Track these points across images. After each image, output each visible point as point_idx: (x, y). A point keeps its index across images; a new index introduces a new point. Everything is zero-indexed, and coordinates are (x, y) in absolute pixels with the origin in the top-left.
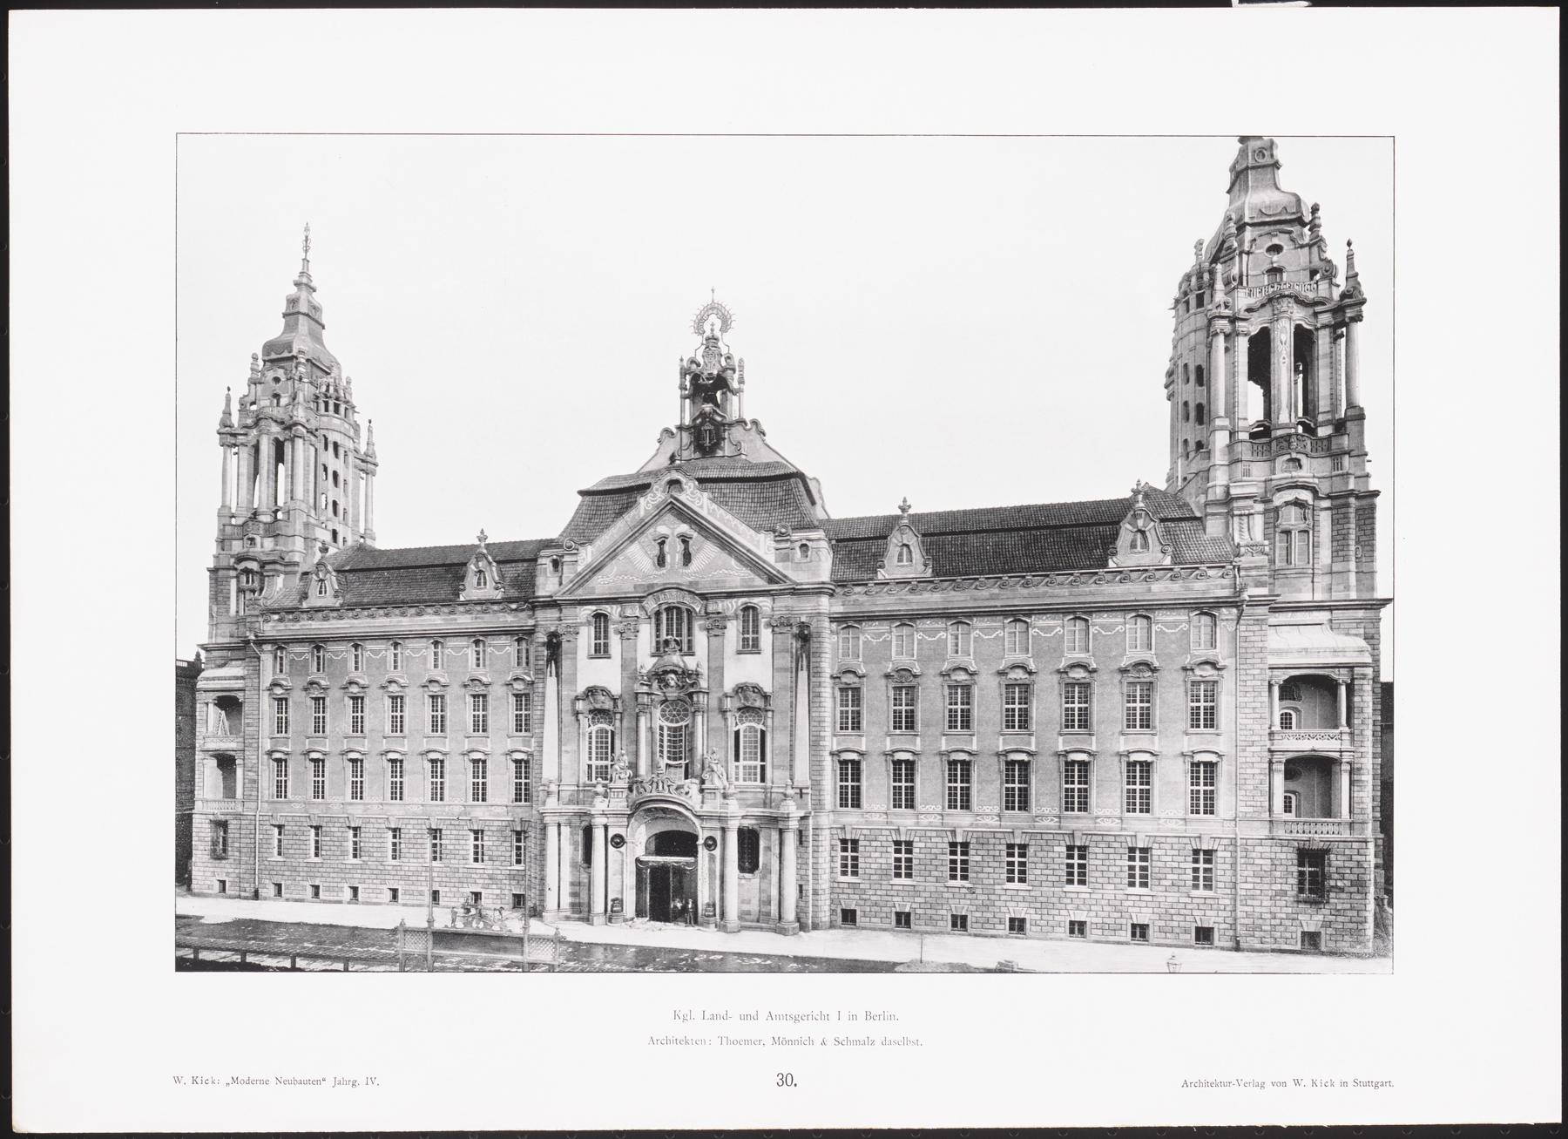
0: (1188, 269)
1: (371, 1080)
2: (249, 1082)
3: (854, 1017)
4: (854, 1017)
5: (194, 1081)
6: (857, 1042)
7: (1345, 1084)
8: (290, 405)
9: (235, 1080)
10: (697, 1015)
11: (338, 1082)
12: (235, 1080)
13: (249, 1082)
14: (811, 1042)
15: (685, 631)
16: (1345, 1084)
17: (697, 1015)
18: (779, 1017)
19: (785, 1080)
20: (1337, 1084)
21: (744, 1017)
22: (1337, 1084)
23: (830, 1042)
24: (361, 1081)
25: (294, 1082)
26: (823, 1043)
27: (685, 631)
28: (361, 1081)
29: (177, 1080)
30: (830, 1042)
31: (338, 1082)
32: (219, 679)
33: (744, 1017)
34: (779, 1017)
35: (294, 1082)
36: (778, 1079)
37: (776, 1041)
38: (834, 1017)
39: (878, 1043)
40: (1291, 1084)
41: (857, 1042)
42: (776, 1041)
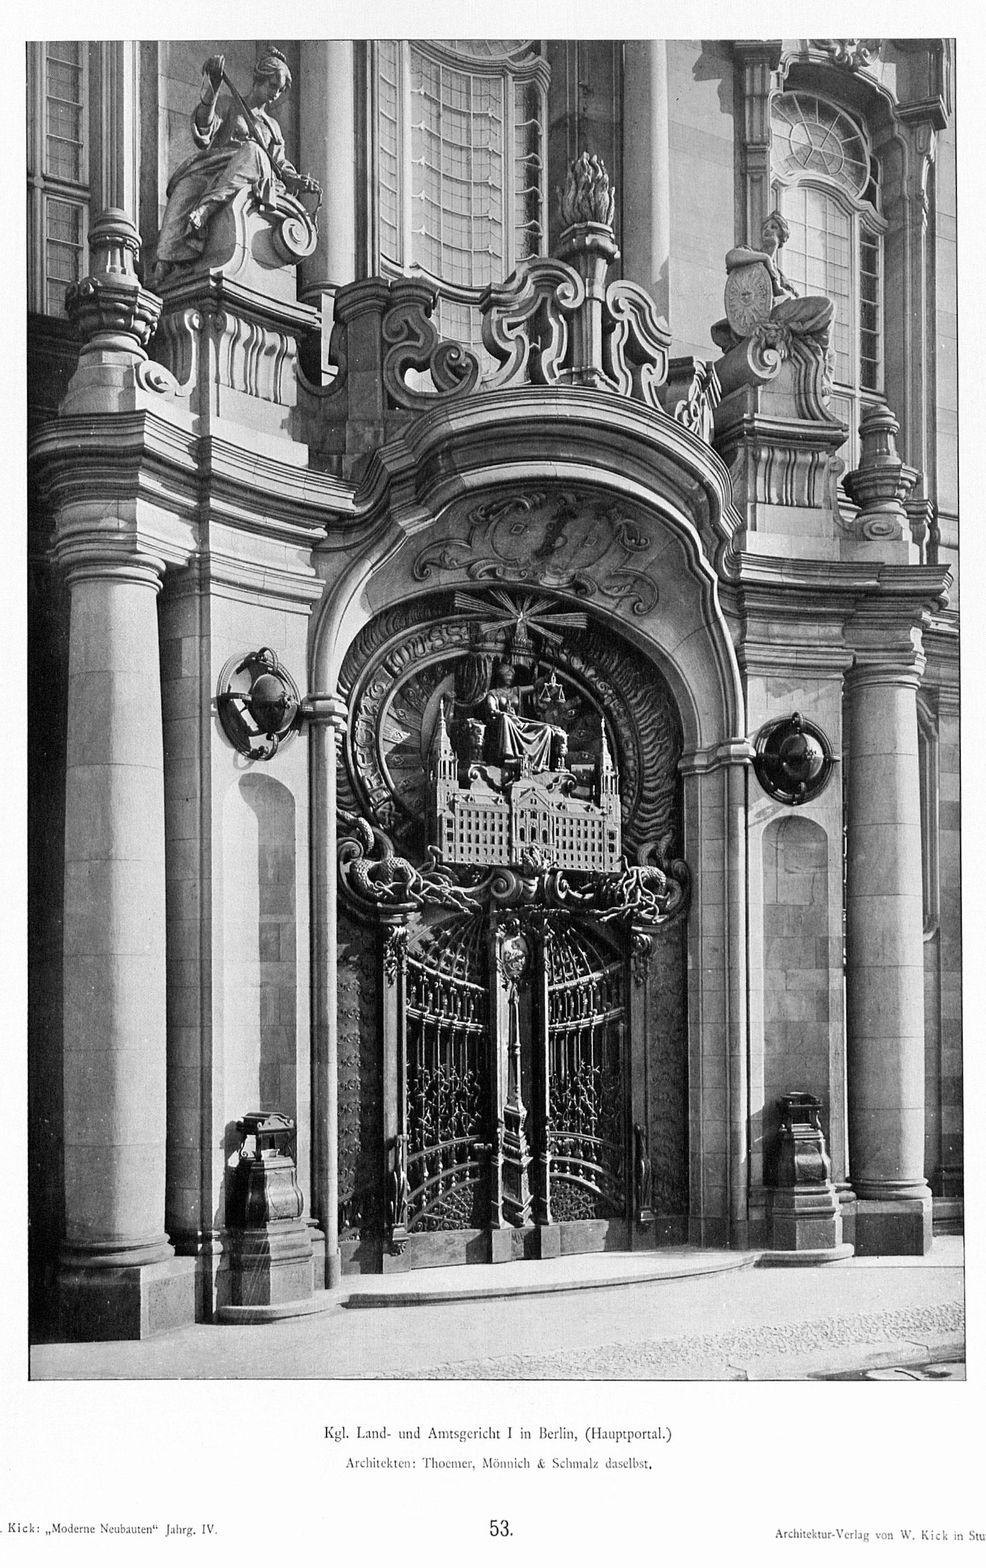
0: (263, 763)
1: (209, 1528)
2: (73, 1529)
3: (527, 1435)
4: (527, 1435)
5: (924, 1536)
6: (577, 1465)
7: (959, 1537)
9: (57, 1528)
10: (351, 1431)
11: (170, 1531)
12: (57, 1528)
13: (73, 1529)
14: (527, 1464)
15: (403, 476)
16: (959, 1537)
17: (351, 1431)
18: (443, 1434)
19: (500, 1529)
20: (951, 1537)
21: (407, 1435)
22: (951, 1537)
23: (548, 1463)
24: (198, 1529)
26: (541, 1466)
27: (403, 476)
28: (198, 1529)
31: (170, 1531)
33: (407, 1435)
34: (443, 1434)
35: (121, 1530)
37: (488, 1463)
39: (601, 1465)
40: (898, 1535)
41: (577, 1465)
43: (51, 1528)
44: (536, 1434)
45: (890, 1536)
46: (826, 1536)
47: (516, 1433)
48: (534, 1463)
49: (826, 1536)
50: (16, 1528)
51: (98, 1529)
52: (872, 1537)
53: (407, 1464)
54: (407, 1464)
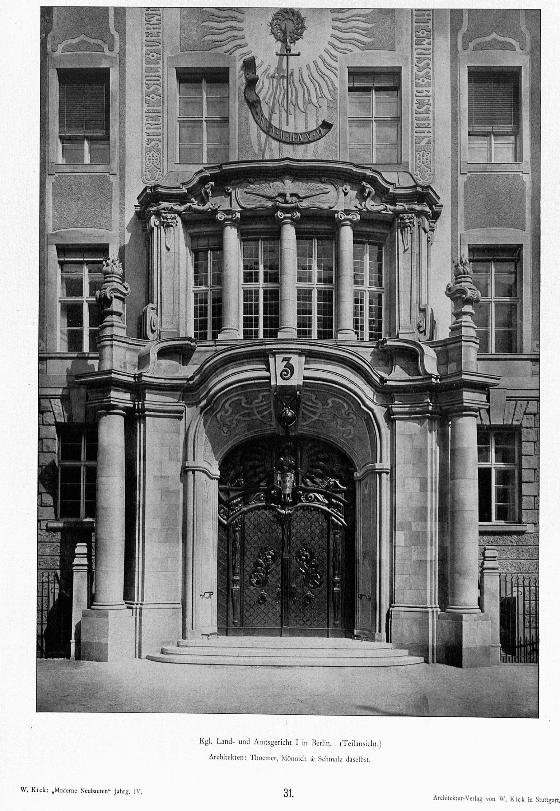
1: (137, 791)
2: (65, 791)
3: (305, 743)
4: (305, 743)
5: (33, 790)
6: (332, 760)
7: (530, 800)
8: (425, 335)
9: (57, 790)
10: (214, 740)
12: (57, 790)
13: (65, 791)
14: (305, 759)
17: (214, 740)
18: (262, 743)
20: (526, 800)
21: (241, 742)
22: (526, 800)
23: (316, 759)
25: (91, 791)
29: (23, 789)
30: (316, 759)
32: (139, 557)
33: (241, 742)
34: (262, 743)
35: (91, 791)
36: (284, 793)
37: (285, 758)
38: (293, 743)
39: (344, 760)
40: (497, 799)
41: (332, 760)
42: (285, 758)
43: (54, 790)
44: (310, 743)
45: (493, 799)
46: (460, 799)
47: (300, 742)
48: (309, 759)
49: (460, 799)
50: (36, 790)
51: (79, 791)
52: (484, 800)
53: (242, 758)
54: (242, 758)
